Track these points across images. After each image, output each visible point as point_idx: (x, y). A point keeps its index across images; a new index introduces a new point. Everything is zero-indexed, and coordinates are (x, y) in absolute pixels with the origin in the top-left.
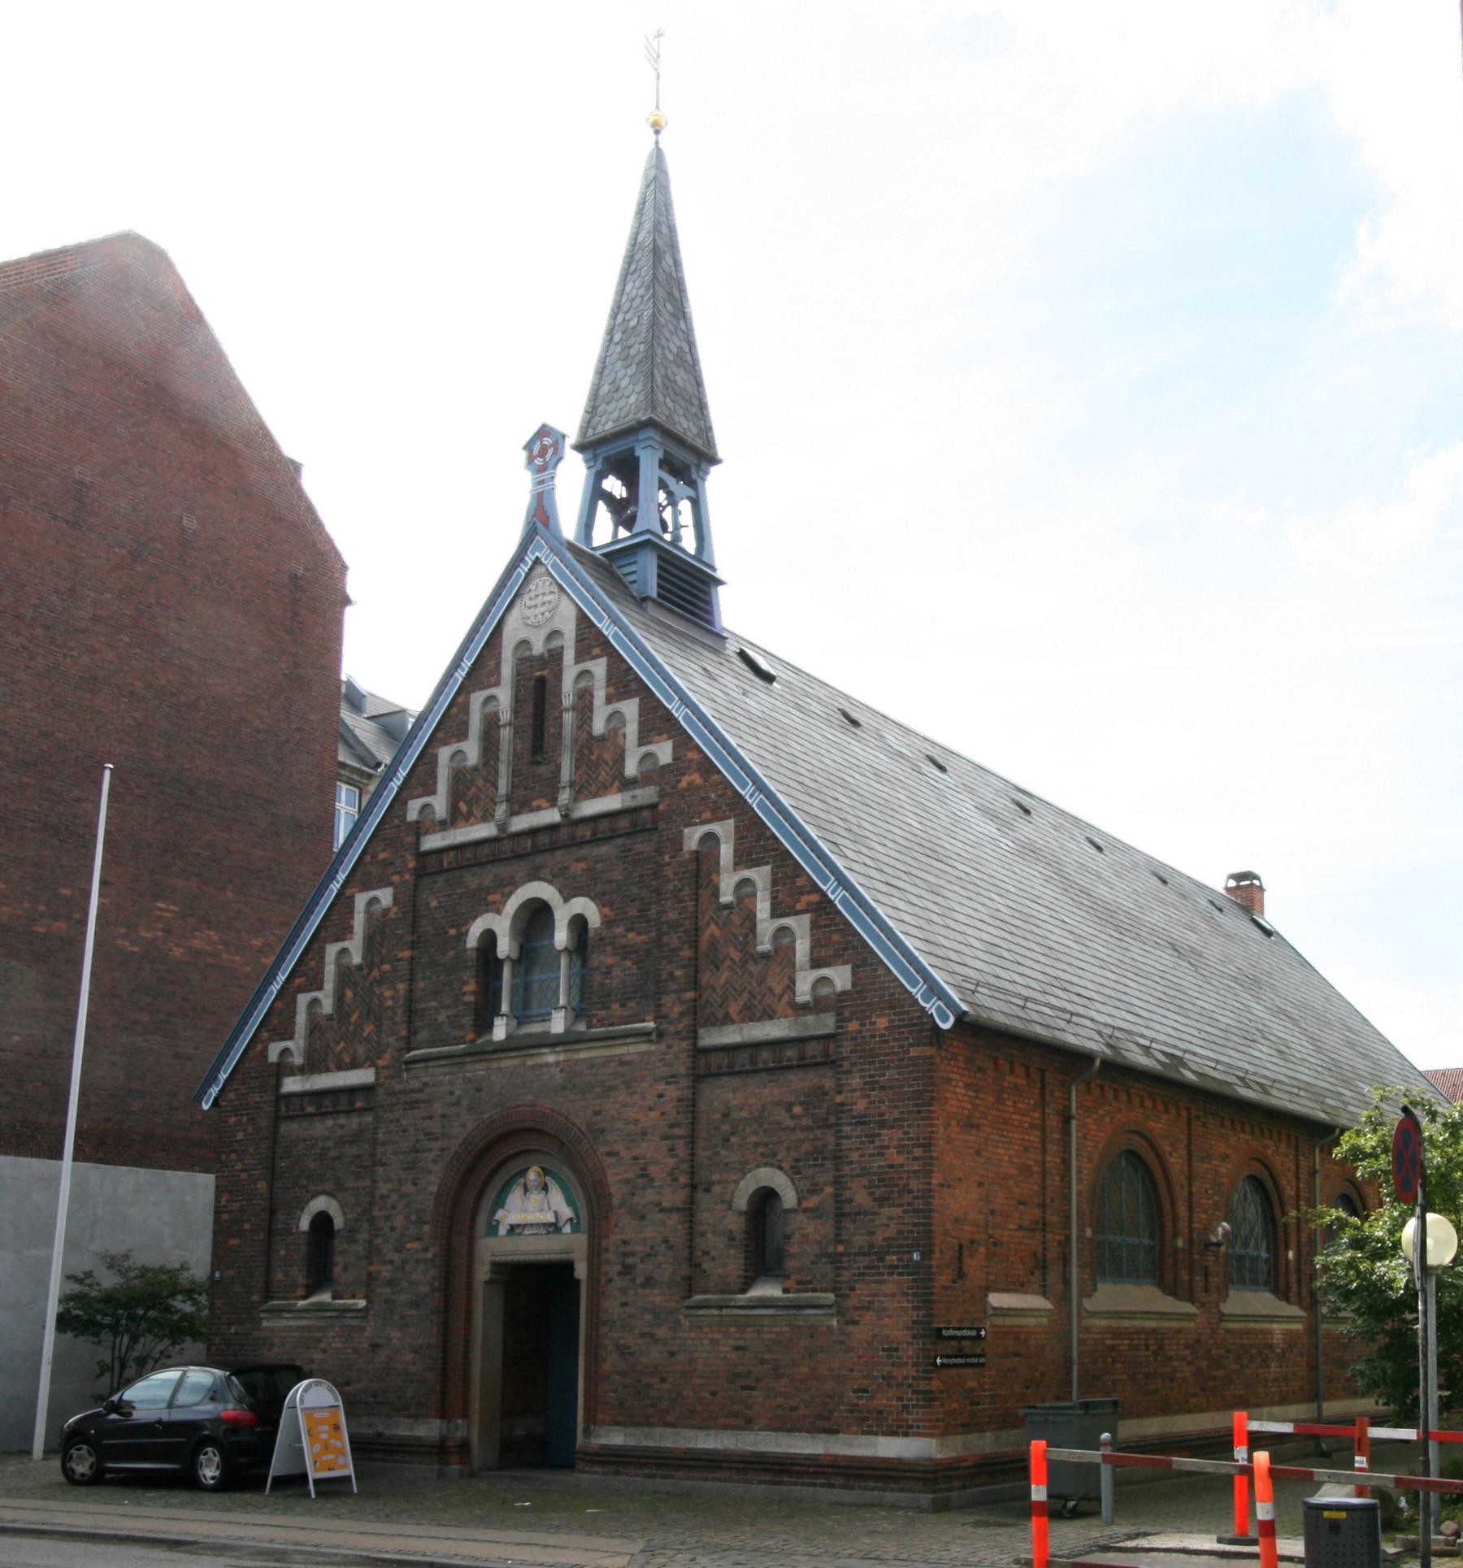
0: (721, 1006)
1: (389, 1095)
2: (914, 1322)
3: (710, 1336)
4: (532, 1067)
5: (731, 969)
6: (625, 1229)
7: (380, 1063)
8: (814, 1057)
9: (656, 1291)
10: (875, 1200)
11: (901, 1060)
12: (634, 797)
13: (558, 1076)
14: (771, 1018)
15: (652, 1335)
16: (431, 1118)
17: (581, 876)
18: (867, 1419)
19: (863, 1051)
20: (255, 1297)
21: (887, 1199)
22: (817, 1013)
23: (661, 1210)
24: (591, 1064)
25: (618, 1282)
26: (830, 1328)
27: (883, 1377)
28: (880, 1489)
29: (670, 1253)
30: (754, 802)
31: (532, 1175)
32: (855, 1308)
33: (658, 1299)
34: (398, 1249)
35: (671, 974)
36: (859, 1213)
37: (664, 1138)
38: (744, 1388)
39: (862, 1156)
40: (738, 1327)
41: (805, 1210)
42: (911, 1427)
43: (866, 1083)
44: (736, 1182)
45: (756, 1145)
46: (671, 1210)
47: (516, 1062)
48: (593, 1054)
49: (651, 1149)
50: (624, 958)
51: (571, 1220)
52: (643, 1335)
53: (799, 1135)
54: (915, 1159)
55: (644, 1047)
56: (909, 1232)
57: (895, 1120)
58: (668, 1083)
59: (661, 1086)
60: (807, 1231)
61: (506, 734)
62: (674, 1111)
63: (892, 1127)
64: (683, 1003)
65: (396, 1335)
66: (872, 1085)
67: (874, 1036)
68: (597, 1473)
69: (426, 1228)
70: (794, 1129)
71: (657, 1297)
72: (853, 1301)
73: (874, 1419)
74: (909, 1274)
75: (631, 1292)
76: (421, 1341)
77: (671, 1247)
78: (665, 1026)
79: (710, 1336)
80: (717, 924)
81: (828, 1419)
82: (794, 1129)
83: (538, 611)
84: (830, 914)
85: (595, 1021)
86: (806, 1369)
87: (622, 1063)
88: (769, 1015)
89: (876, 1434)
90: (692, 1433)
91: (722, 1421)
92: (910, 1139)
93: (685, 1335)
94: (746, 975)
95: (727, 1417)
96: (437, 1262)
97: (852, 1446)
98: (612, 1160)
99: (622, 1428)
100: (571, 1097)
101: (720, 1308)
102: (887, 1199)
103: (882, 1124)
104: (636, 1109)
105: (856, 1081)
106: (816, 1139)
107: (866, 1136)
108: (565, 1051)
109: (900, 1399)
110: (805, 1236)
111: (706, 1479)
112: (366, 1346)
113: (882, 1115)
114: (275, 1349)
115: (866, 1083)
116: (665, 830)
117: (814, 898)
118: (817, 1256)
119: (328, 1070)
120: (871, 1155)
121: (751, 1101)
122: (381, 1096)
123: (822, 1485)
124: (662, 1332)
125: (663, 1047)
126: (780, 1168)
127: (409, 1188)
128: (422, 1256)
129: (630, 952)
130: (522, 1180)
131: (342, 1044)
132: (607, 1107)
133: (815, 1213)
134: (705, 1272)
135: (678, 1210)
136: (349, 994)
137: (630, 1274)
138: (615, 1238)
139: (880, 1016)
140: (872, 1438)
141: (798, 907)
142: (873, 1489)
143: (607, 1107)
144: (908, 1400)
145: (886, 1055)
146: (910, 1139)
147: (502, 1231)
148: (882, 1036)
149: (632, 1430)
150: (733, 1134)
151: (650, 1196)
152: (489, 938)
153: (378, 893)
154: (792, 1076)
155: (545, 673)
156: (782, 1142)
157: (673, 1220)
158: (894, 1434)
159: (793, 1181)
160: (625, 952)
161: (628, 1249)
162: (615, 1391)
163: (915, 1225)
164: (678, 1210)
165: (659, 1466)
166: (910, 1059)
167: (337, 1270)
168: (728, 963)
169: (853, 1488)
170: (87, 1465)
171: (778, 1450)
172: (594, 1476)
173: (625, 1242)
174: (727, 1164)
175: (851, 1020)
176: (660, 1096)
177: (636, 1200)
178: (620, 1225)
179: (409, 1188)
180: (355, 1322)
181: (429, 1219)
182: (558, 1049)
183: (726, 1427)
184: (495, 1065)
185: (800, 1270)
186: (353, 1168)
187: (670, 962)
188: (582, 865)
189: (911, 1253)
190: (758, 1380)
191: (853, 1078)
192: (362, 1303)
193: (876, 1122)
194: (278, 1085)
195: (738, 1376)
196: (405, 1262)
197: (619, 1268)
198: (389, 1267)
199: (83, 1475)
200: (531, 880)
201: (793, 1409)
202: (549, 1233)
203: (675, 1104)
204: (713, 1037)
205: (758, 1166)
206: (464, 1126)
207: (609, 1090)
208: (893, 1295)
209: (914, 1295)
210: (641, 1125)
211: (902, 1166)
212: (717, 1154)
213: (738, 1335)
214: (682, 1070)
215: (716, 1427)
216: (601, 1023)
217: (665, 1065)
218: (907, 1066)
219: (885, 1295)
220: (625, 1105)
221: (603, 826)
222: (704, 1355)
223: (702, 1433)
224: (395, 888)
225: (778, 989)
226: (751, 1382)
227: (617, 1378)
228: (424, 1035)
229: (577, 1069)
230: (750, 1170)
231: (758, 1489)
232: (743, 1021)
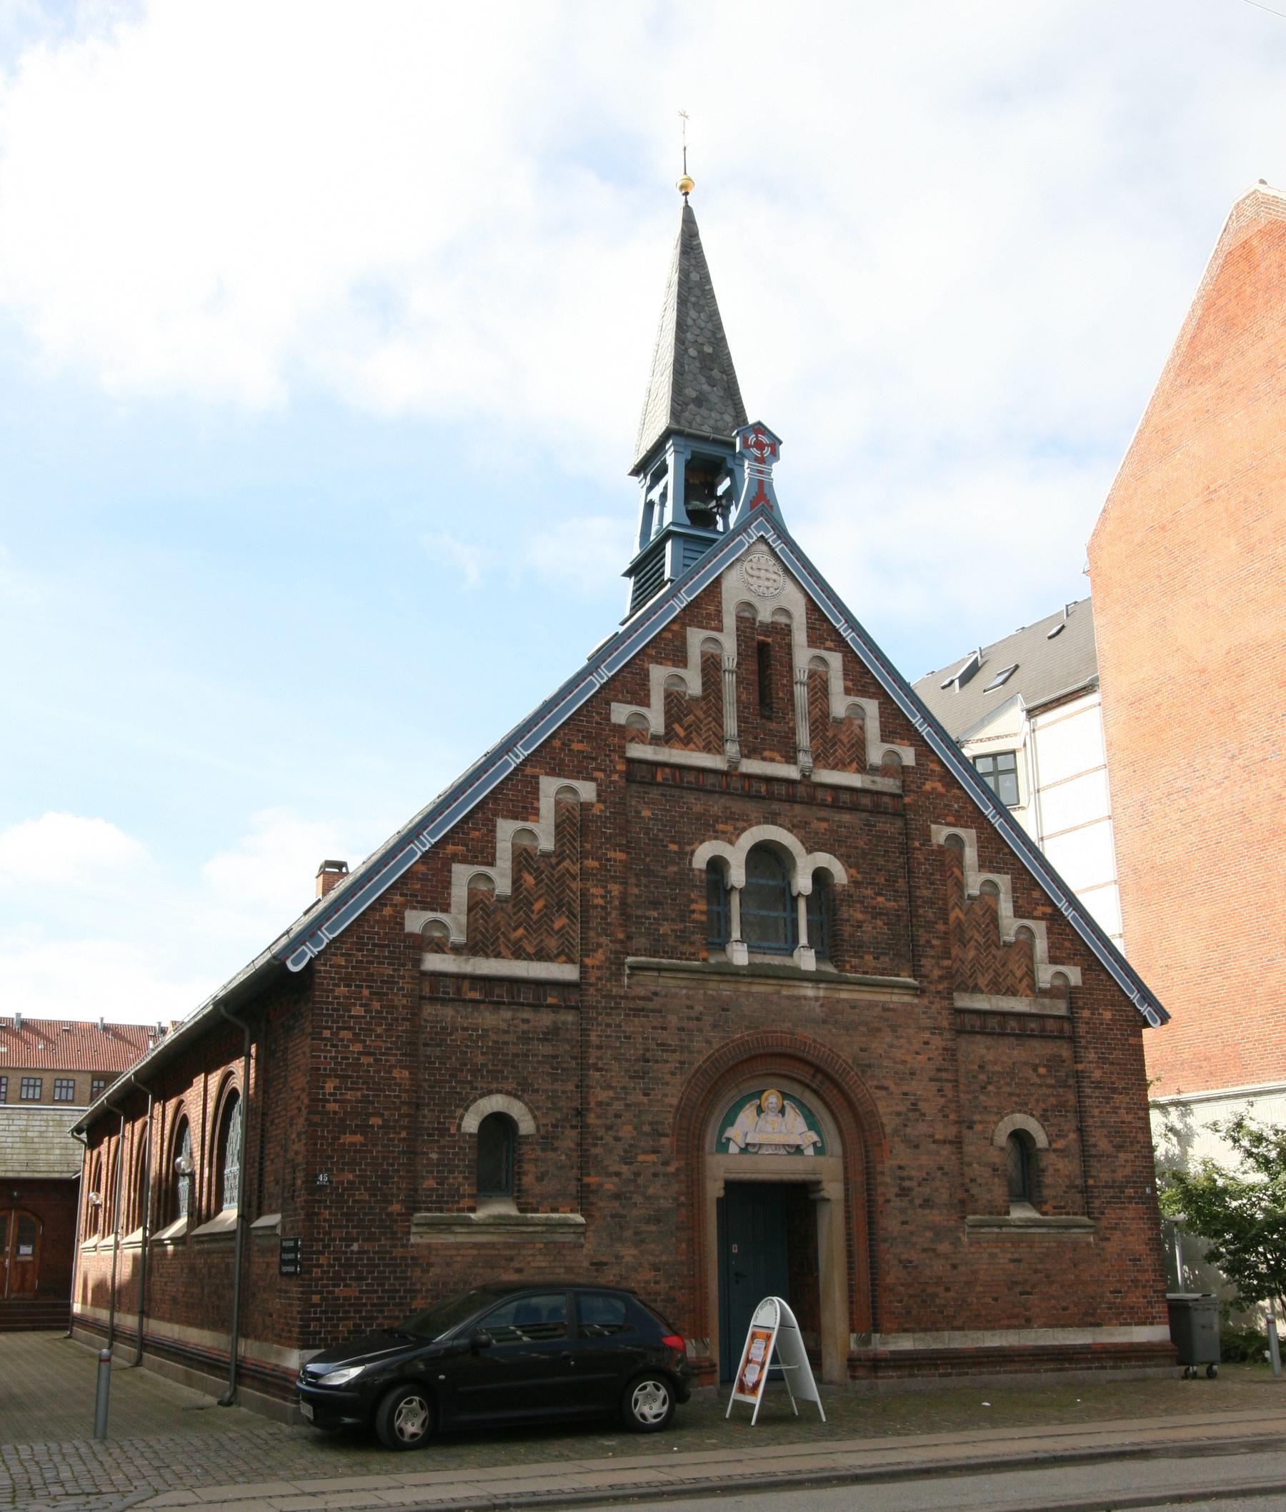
0: (970, 976)
1: (604, 997)
2: (1149, 1239)
3: (988, 1250)
4: (789, 997)
5: (976, 949)
6: (896, 1157)
7: (588, 961)
8: (1051, 1031)
9: (935, 1212)
10: (1114, 1147)
11: (1124, 1045)
12: (873, 782)
13: (818, 1010)
14: (1014, 995)
15: (934, 1250)
16: (664, 1029)
17: (823, 834)
18: (1123, 1314)
19: (1095, 1033)
20: (396, 1208)
21: (1122, 1147)
22: (1051, 998)
23: (934, 1142)
24: (853, 1005)
25: (897, 1203)
26: (1088, 1244)
27: (1132, 1281)
28: (1140, 1367)
29: (945, 1179)
30: (523, 754)
31: (772, 1099)
32: (1106, 1228)
33: (938, 1219)
34: (626, 1161)
35: (928, 942)
36: (1102, 1156)
37: (931, 1080)
38: (1021, 1294)
39: (1101, 1112)
40: (1013, 1243)
41: (1055, 1151)
42: (1155, 1318)
43: (1099, 1058)
44: (996, 1123)
45: (1010, 1094)
46: (944, 1142)
47: (769, 989)
48: (855, 996)
49: (919, 1087)
50: (874, 918)
51: (814, 1144)
52: (924, 1250)
53: (1046, 1091)
54: (1139, 1118)
55: (907, 999)
56: (1141, 1172)
57: (1123, 1088)
58: (933, 1034)
59: (927, 1035)
60: (1058, 1167)
61: (729, 680)
62: (940, 1058)
63: (1121, 1094)
64: (941, 968)
65: (629, 1253)
66: (1103, 1060)
67: (1102, 1024)
68: (891, 1377)
69: (665, 1141)
70: (1041, 1086)
71: (935, 1216)
72: (1104, 1223)
73: (1128, 1313)
74: (1143, 1203)
75: (910, 1212)
76: (664, 1258)
77: (945, 1174)
78: (925, 984)
79: (988, 1250)
80: (961, 909)
81: (1093, 1315)
82: (1041, 1086)
83: (760, 582)
84: (1060, 925)
85: (848, 967)
86: (1073, 1277)
87: (886, 1010)
88: (1013, 992)
89: (1130, 1324)
90: (979, 1334)
91: (1005, 1322)
92: (1135, 1104)
93: (966, 1250)
94: (990, 957)
95: (1009, 1318)
96: (682, 1177)
98: (883, 1093)
99: (910, 1335)
101: (1000, 1227)
102: (1122, 1147)
103: (1114, 1090)
104: (903, 1051)
105: (1092, 1056)
106: (1059, 1095)
107: (1103, 1098)
108: (826, 989)
109: (1145, 1297)
110: (1057, 1170)
111: (999, 1373)
112: (586, 1264)
113: (1113, 1083)
114: (434, 1271)
115: (1099, 1058)
116: (912, 819)
117: (1049, 910)
118: (1067, 1187)
119: (498, 955)
120: (1108, 1112)
121: (1004, 1058)
122: (592, 996)
123: (1097, 1368)
124: (944, 1247)
125: (925, 1001)
126: (1032, 1115)
127: (637, 1097)
128: (661, 1169)
129: (881, 914)
130: (757, 1102)
131: (521, 931)
132: (874, 1046)
133: (1062, 1153)
134: (973, 1196)
135: (951, 1142)
136: (529, 880)
137: (907, 1196)
138: (890, 1163)
139: (1106, 1010)
140: (1128, 1328)
141: (1036, 913)
142: (1135, 1367)
144: (1151, 1297)
145: (1112, 1039)
146: (1135, 1104)
147: (733, 1149)
148: (1107, 1024)
149: (921, 1335)
150: (990, 1083)
151: (922, 1128)
152: (717, 866)
153: (576, 784)
154: (1035, 1043)
155: (770, 640)
156: (1032, 1095)
157: (946, 1150)
158: (1144, 1324)
159: (1043, 1126)
160: (876, 913)
161: (905, 1174)
162: (901, 1301)
163: (1144, 1167)
164: (951, 1142)
165: (953, 1366)
166: (1130, 1045)
167: (528, 1180)
168: (973, 943)
169: (1120, 1368)
170: (419, 1421)
171: (1056, 1343)
172: (891, 1381)
173: (900, 1168)
174: (985, 1108)
175: (1084, 1009)
176: (926, 1043)
177: (908, 1130)
178: (894, 1152)
179: (637, 1097)
180: (569, 1238)
182: (822, 985)
183: (1009, 1327)
184: (744, 988)
185: (1055, 1197)
186: (547, 1069)
187: (929, 932)
188: (824, 825)
189: (1144, 1188)
190: (1033, 1286)
191: (1089, 1053)
192: (578, 1218)
193: (1109, 1088)
194: (418, 962)
195: (1016, 1283)
196: (637, 1174)
197: (896, 1190)
198: (616, 1180)
199: (414, 1435)
200: (766, 822)
201: (1065, 1309)
202: (789, 1153)
203: (941, 1052)
204: (965, 1001)
205: (1013, 1112)
206: (708, 1042)
207: (873, 1032)
208: (1134, 1219)
209: (1148, 1219)
210: (908, 1066)
211: (1130, 1123)
212: (976, 1098)
213: (1013, 1250)
214: (945, 1024)
215: (1001, 1327)
216: (855, 969)
217: (929, 1018)
218: (1129, 1050)
219: (1127, 1219)
220: (891, 1046)
221: (691, 777)
222: (985, 1267)
223: (988, 1334)
224: (599, 785)
225: (1019, 974)
226: (1028, 1289)
227: (902, 1289)
228: (641, 942)
229: (840, 1006)
230: (1007, 1114)
231: (1047, 1377)
232: (990, 992)
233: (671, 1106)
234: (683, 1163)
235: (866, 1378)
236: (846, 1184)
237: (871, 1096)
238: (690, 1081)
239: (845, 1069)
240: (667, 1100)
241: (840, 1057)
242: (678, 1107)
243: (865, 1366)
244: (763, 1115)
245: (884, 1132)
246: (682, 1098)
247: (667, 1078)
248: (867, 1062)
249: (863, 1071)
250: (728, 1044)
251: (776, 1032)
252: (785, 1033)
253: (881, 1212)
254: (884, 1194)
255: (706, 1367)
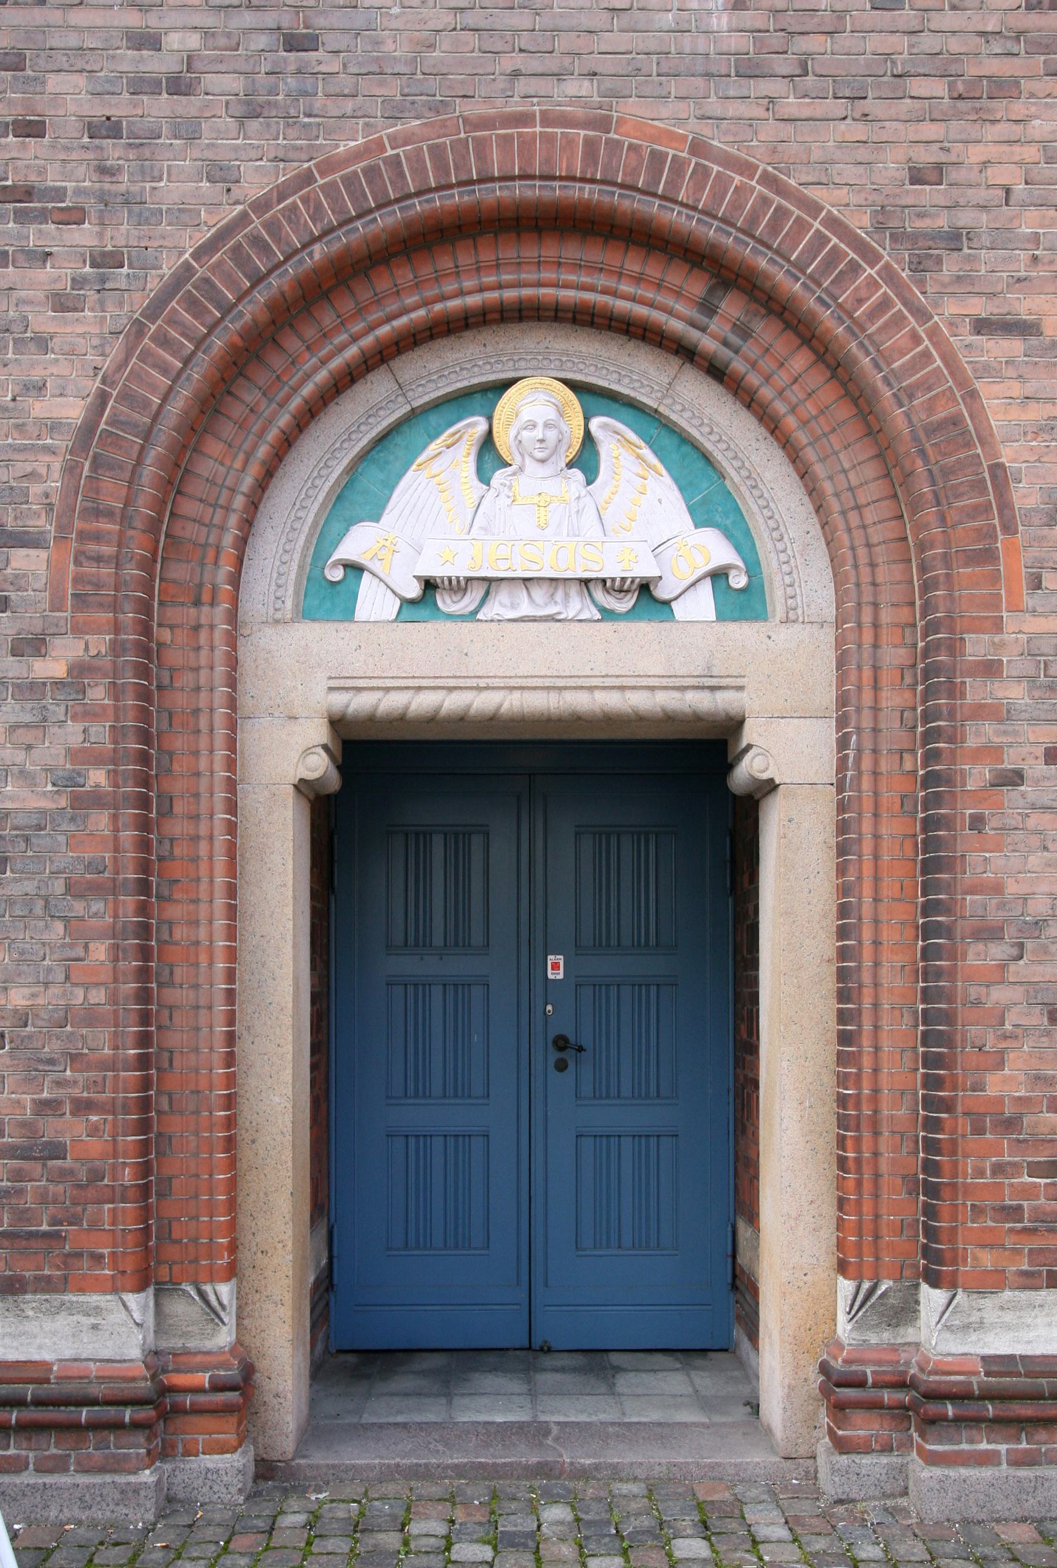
16: (32, 129)
51: (718, 576)
96: (98, 694)
97: (981, 1325)
98: (1013, 346)
100: (792, 105)
143: (976, 154)
172: (987, 1473)
181: (44, 524)
202: (607, 615)
233: (54, 427)
234: (100, 643)
235: (887, 1449)
236: (842, 722)
237: (950, 359)
238: (139, 329)
239: (781, 213)
240: (39, 408)
241: (814, 209)
242: (87, 430)
243: (875, 1406)
244: (499, 477)
245: (1005, 505)
246: (103, 398)
247: (44, 320)
248: (942, 222)
249: (918, 266)
250: (307, 178)
251: (524, 119)
252: (565, 121)
253: (977, 822)
254: (993, 752)
255: (199, 1390)
